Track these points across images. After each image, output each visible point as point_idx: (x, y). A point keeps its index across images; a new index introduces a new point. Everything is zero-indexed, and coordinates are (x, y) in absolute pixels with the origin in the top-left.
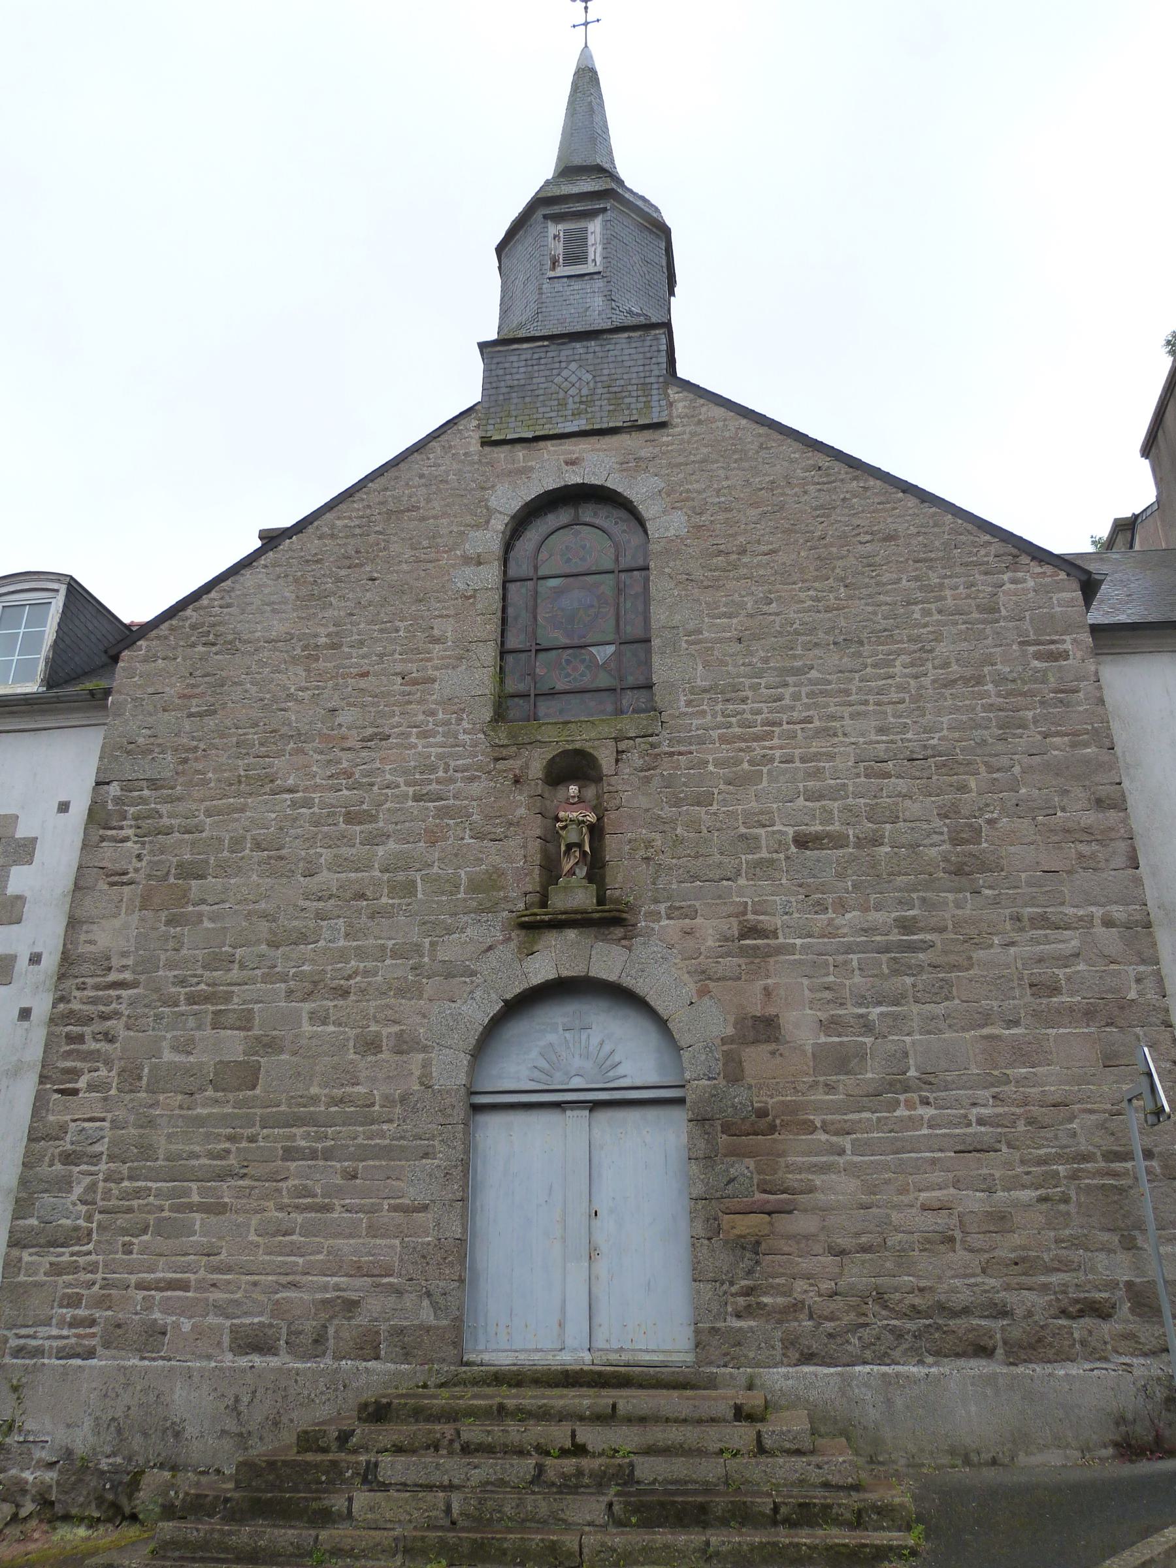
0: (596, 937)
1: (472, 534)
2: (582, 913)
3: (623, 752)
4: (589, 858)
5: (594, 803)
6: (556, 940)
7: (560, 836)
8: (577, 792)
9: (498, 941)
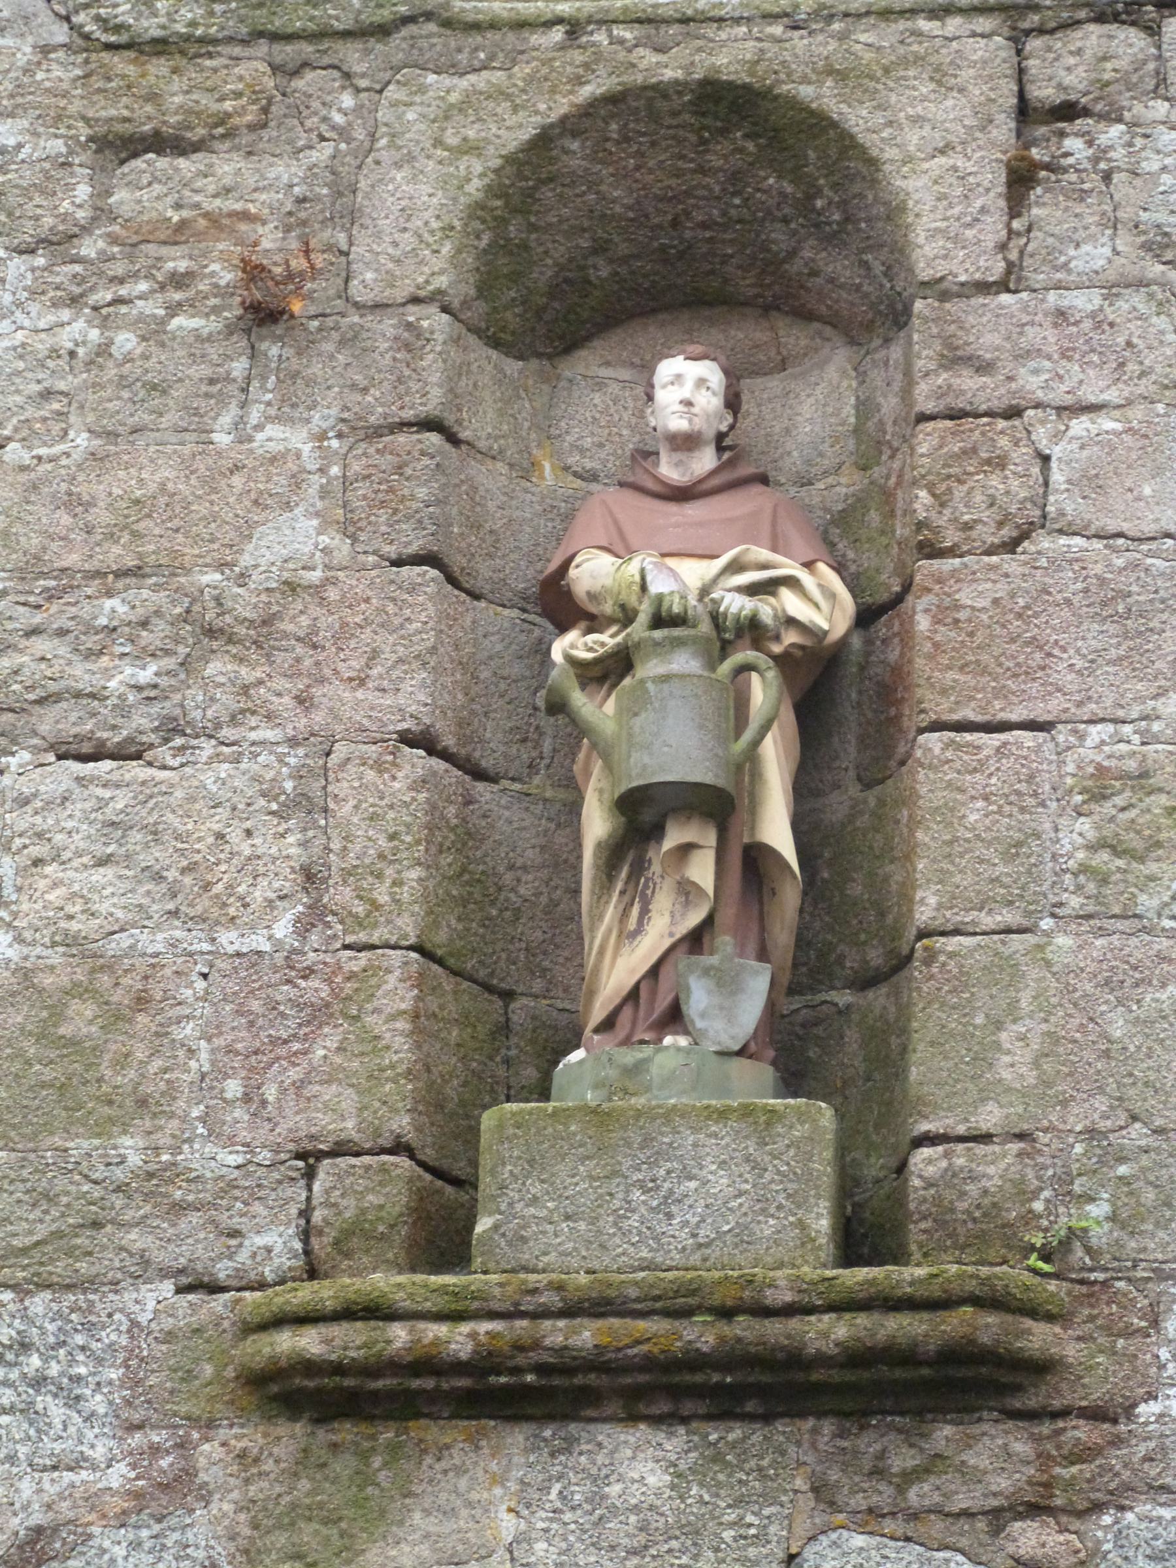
0: (820, 1490)
1: (93, 255)
2: (726, 1313)
3: (1068, 111)
4: (790, 897)
5: (847, 484)
6: (522, 1506)
7: (578, 731)
8: (710, 401)
9: (93, 1500)
